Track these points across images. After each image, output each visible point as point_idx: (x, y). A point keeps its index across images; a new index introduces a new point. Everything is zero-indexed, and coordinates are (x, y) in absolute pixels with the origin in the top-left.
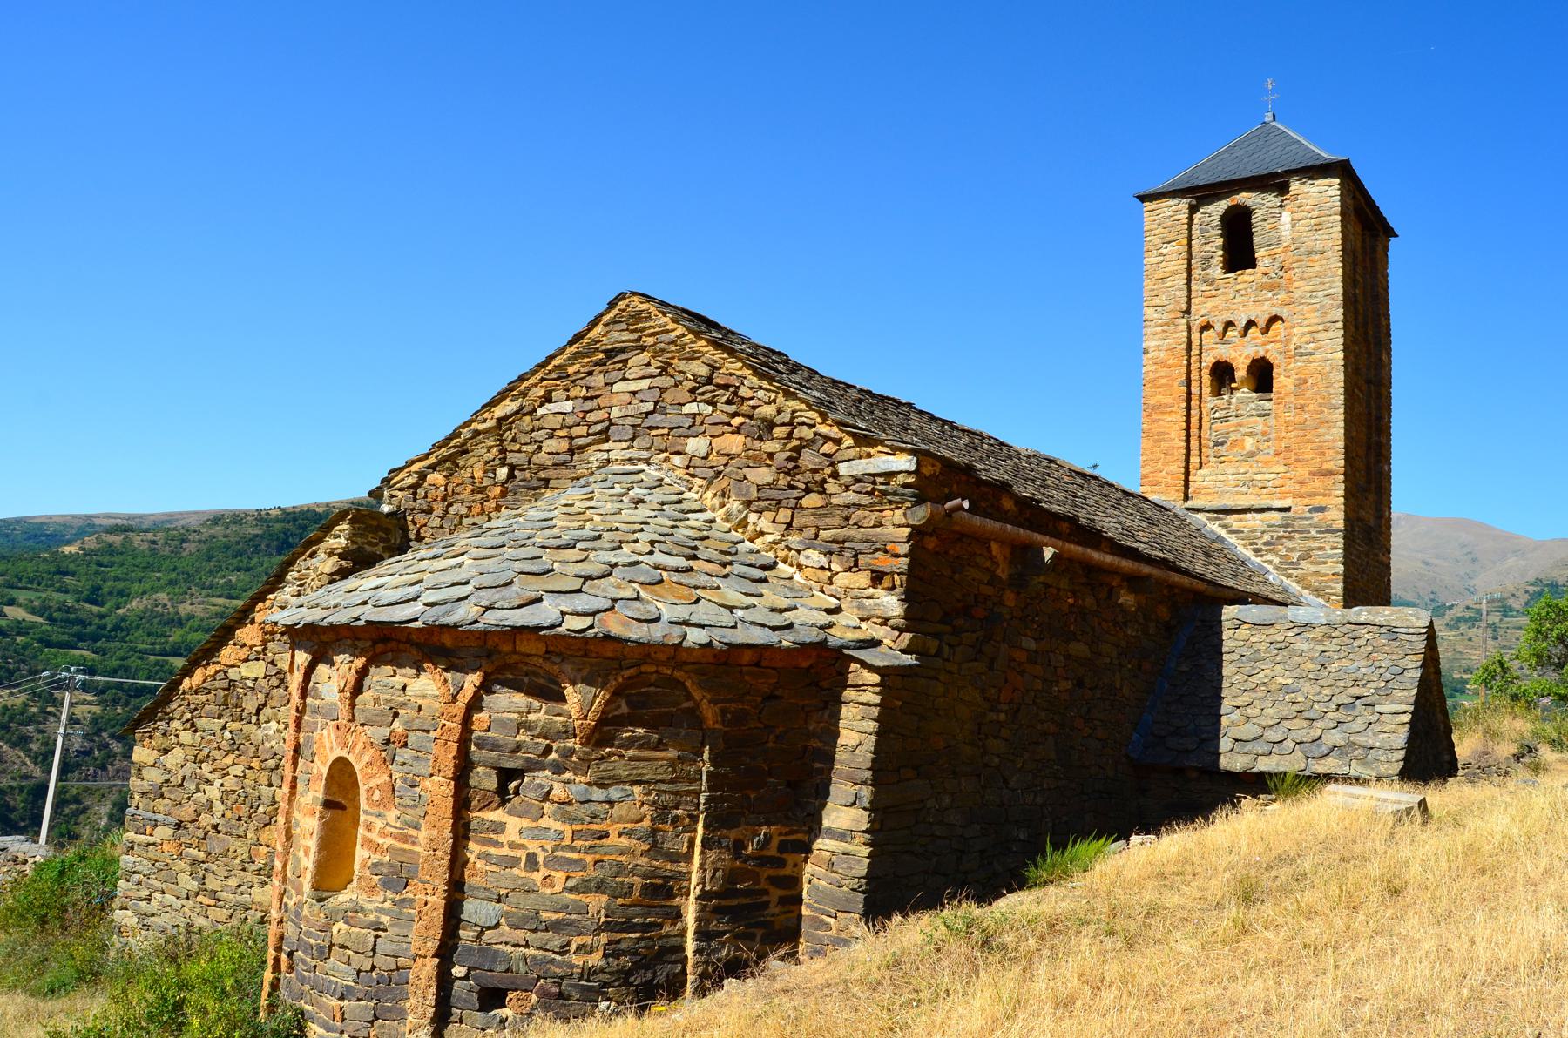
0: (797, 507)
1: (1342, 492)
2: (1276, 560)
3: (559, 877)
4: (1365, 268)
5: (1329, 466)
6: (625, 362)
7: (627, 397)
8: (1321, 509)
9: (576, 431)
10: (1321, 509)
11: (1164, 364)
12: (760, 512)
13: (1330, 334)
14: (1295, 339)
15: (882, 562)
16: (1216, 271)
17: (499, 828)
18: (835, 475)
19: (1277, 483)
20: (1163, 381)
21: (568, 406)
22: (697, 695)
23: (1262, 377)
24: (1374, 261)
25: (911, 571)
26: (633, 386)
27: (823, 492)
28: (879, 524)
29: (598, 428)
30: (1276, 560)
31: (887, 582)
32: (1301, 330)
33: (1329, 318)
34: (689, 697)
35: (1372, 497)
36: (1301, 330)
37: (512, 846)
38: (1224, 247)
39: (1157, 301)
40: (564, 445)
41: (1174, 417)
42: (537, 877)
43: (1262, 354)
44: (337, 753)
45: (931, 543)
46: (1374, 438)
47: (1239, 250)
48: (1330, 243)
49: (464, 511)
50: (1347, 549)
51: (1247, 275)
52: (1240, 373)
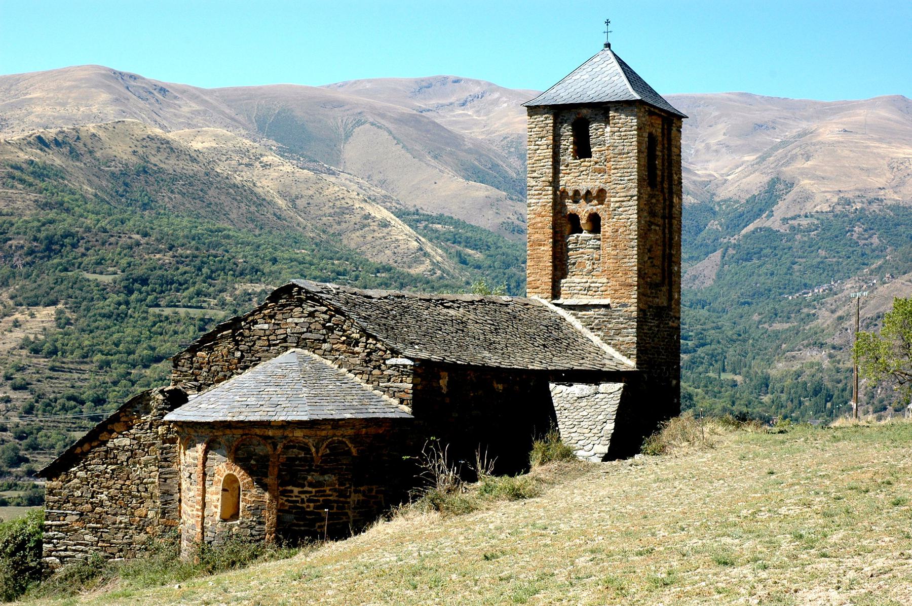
0: (371, 374)
1: (636, 296)
2: (602, 334)
3: (312, 505)
4: (663, 145)
5: (630, 281)
6: (292, 310)
7: (294, 325)
8: (625, 305)
9: (271, 338)
10: (625, 305)
11: (539, 215)
12: (356, 374)
13: (630, 203)
14: (612, 204)
15: (402, 395)
16: (570, 159)
17: (292, 491)
18: (384, 363)
19: (602, 289)
20: (540, 225)
21: (266, 326)
22: (350, 445)
23: (595, 222)
24: (670, 140)
25: (414, 399)
26: (296, 320)
27: (380, 369)
28: (401, 382)
29: (282, 337)
30: (602, 334)
31: (405, 402)
32: (615, 199)
33: (630, 193)
34: (347, 446)
35: (664, 289)
36: (615, 199)
37: (296, 496)
38: (574, 143)
39: (535, 175)
40: (266, 343)
41: (545, 248)
42: (305, 505)
43: (595, 211)
44: (228, 472)
45: (419, 387)
46: (667, 251)
47: (583, 150)
48: (631, 148)
49: (219, 369)
50: (639, 328)
51: (586, 162)
52: (583, 222)
